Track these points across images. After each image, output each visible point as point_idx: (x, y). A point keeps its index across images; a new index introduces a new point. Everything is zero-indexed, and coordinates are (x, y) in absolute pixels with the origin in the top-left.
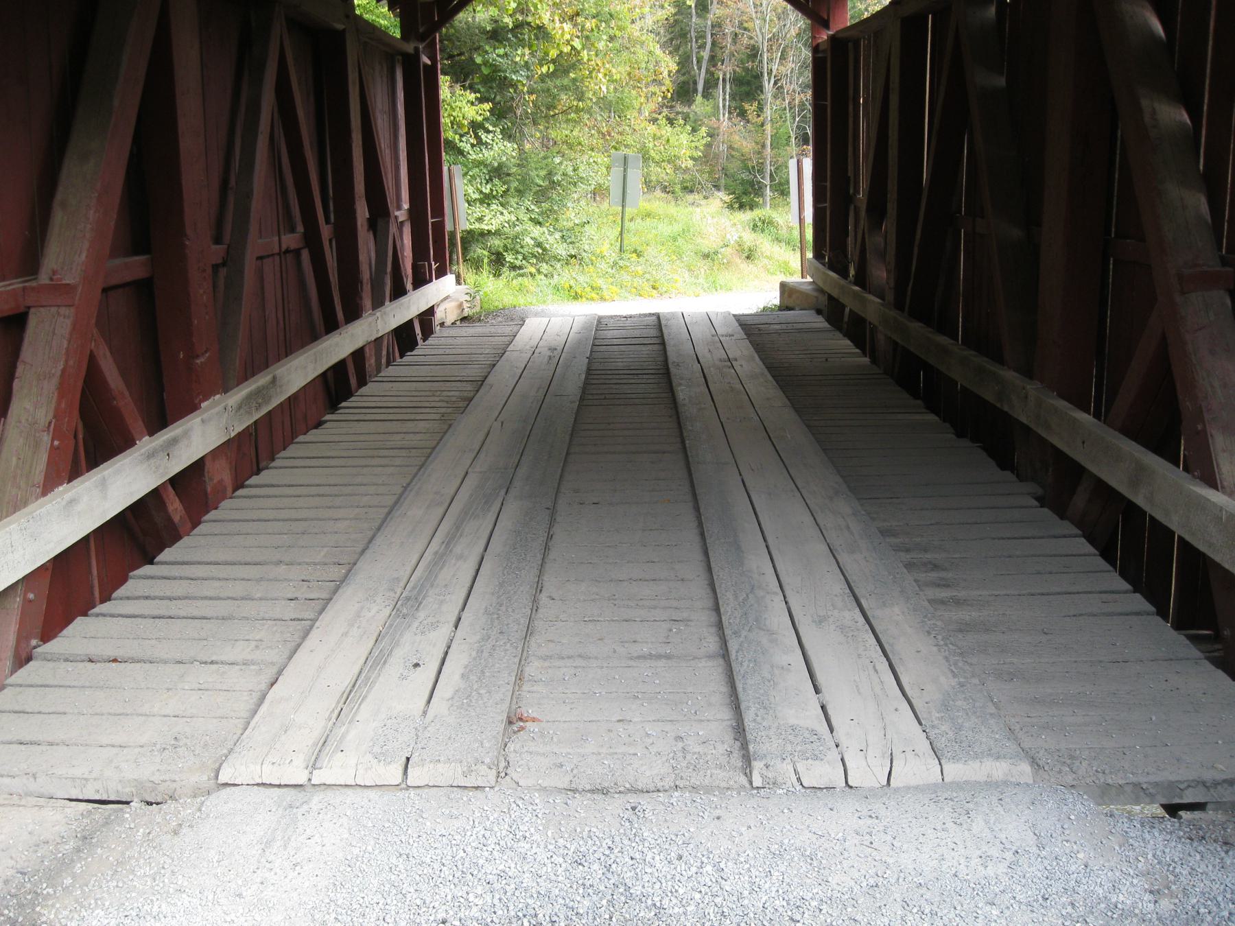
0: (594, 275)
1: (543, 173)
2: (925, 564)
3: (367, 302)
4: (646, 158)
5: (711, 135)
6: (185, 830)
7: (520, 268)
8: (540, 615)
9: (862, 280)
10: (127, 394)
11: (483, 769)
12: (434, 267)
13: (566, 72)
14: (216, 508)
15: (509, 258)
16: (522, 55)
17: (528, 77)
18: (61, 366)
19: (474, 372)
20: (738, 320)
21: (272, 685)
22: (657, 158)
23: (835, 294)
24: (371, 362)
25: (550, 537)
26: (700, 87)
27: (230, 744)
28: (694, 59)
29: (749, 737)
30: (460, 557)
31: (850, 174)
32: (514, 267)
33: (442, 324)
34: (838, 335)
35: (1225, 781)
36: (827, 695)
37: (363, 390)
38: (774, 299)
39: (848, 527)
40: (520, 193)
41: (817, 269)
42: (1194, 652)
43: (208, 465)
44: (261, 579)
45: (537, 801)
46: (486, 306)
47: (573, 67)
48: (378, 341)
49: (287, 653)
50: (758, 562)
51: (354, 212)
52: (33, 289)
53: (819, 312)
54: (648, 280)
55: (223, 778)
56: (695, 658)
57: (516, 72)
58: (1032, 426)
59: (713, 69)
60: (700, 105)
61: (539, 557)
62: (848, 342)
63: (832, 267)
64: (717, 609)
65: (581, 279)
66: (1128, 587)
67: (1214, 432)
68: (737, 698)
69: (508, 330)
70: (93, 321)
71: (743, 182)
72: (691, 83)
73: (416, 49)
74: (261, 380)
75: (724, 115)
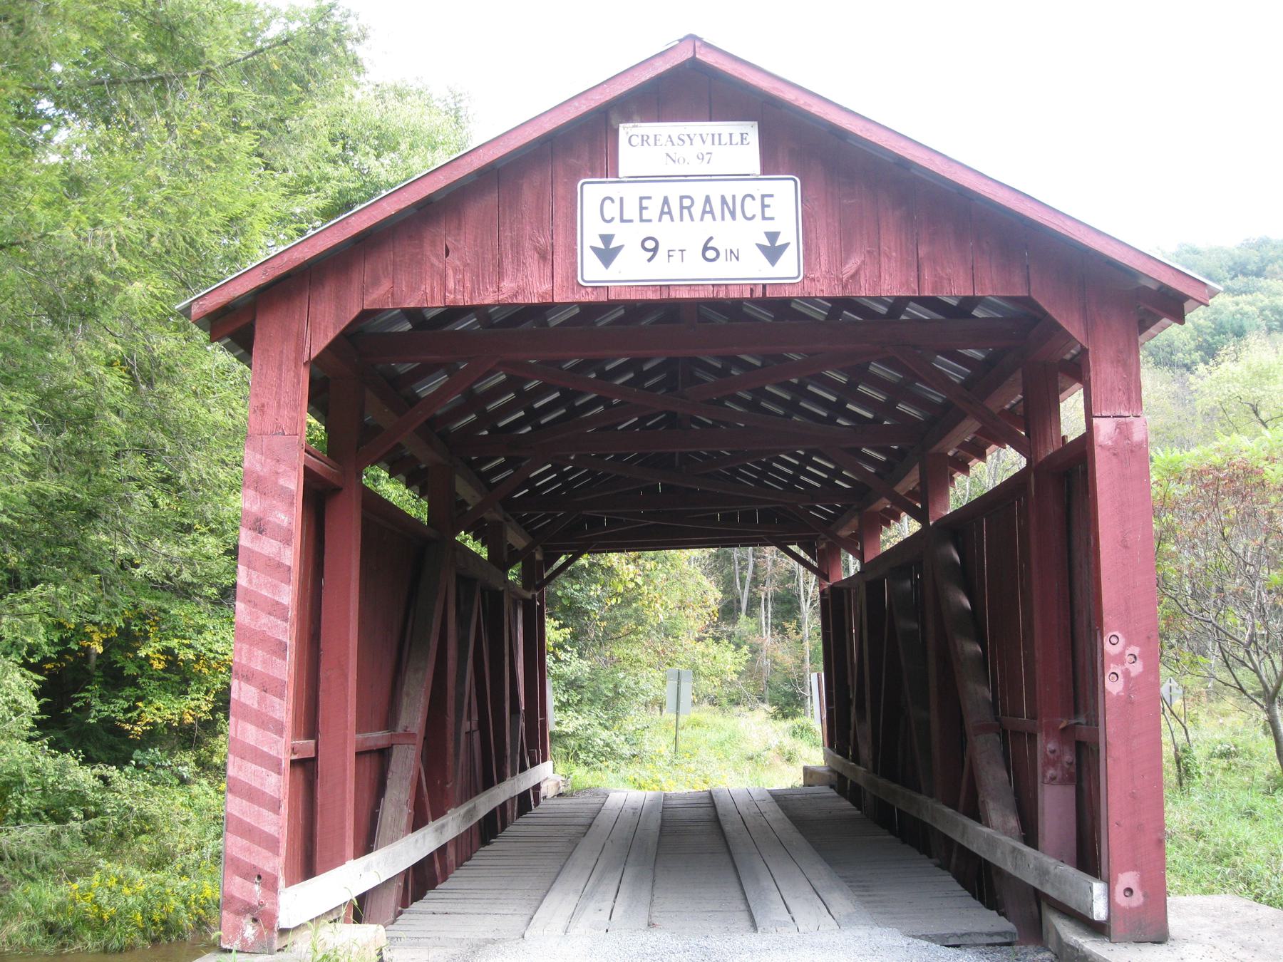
0: (655, 770)
4: (696, 673)
9: (856, 759)
15: (582, 756)
16: (595, 591)
20: (772, 795)
22: (706, 672)
26: (744, 605)
28: (738, 580)
34: (843, 799)
37: (504, 834)
40: (592, 702)
41: (829, 754)
47: (635, 599)
53: (832, 787)
54: (699, 776)
57: (590, 603)
59: (755, 590)
60: (744, 624)
62: (848, 803)
65: (643, 773)
71: (785, 694)
72: (735, 602)
73: (534, 596)
75: (766, 631)
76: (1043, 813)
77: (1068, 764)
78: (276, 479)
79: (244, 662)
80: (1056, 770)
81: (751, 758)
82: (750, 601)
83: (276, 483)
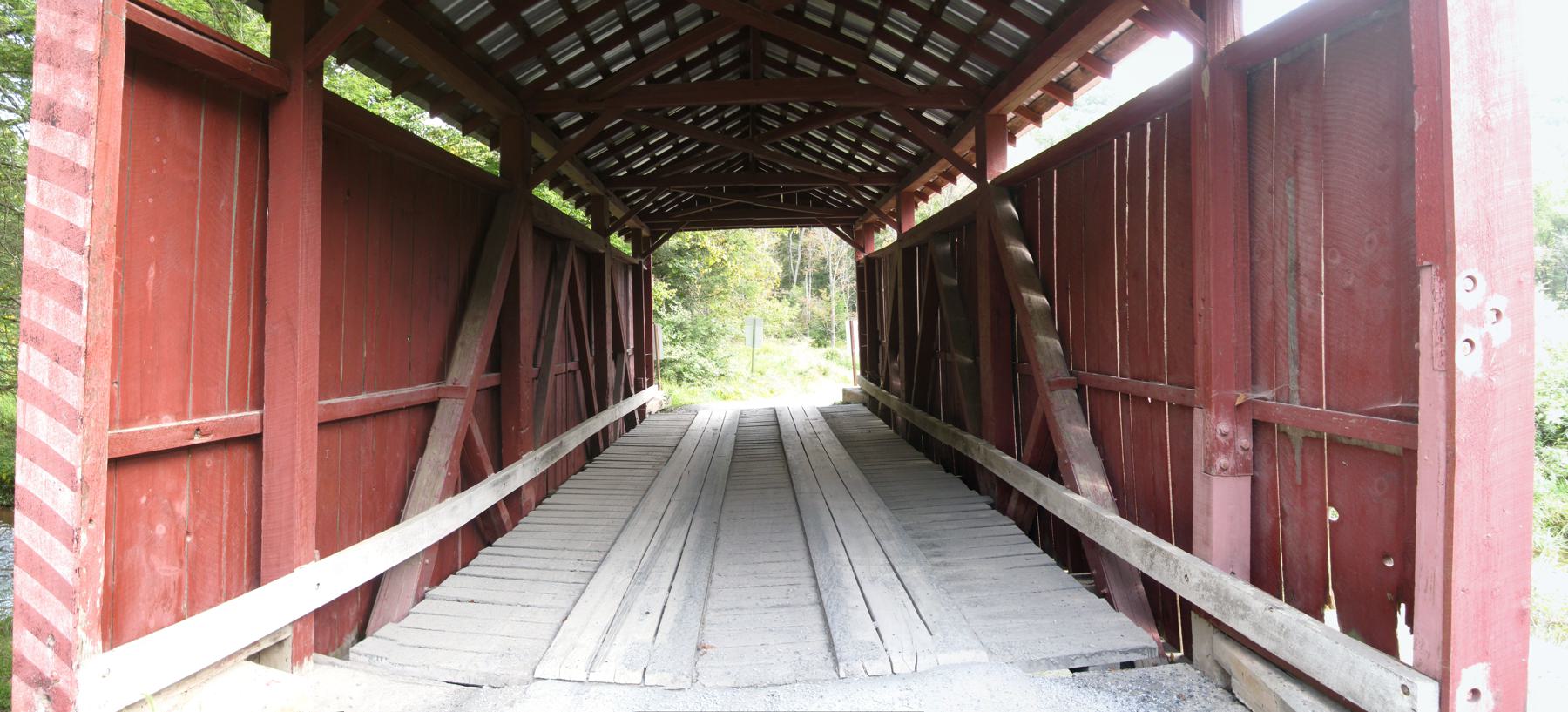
1: (705, 328)
2: (929, 545)
3: (611, 400)
5: (801, 307)
6: (517, 704)
7: (692, 381)
8: (713, 585)
9: (887, 387)
10: (485, 449)
11: (684, 678)
12: (646, 380)
13: (719, 273)
14: (526, 516)
16: (694, 263)
17: (697, 275)
18: (456, 431)
19: (670, 441)
20: (820, 411)
21: (564, 621)
23: (873, 394)
24: (611, 434)
25: (717, 539)
26: (795, 280)
27: (541, 655)
29: (836, 649)
30: (669, 550)
31: (879, 329)
32: (688, 381)
33: (650, 413)
34: (876, 417)
35: (1096, 653)
36: (879, 622)
37: (607, 450)
38: (840, 398)
39: (886, 526)
40: (692, 339)
41: (863, 381)
42: (1078, 584)
43: (524, 491)
44: (555, 558)
45: (717, 695)
46: (674, 403)
48: (616, 422)
49: (571, 603)
50: (836, 548)
51: (606, 350)
52: (443, 388)
53: (865, 405)
55: (536, 676)
56: (804, 606)
58: (983, 464)
61: (712, 551)
62: (881, 421)
63: (871, 380)
64: (815, 577)
65: (728, 387)
66: (1040, 550)
67: (1074, 463)
68: (829, 627)
69: (689, 417)
70: (471, 408)
73: (640, 262)
74: (554, 443)
76: (1208, 511)
77: (1243, 449)
78: (73, 41)
79: (33, 318)
80: (1228, 458)
81: (801, 374)
82: (799, 277)
83: (72, 48)
